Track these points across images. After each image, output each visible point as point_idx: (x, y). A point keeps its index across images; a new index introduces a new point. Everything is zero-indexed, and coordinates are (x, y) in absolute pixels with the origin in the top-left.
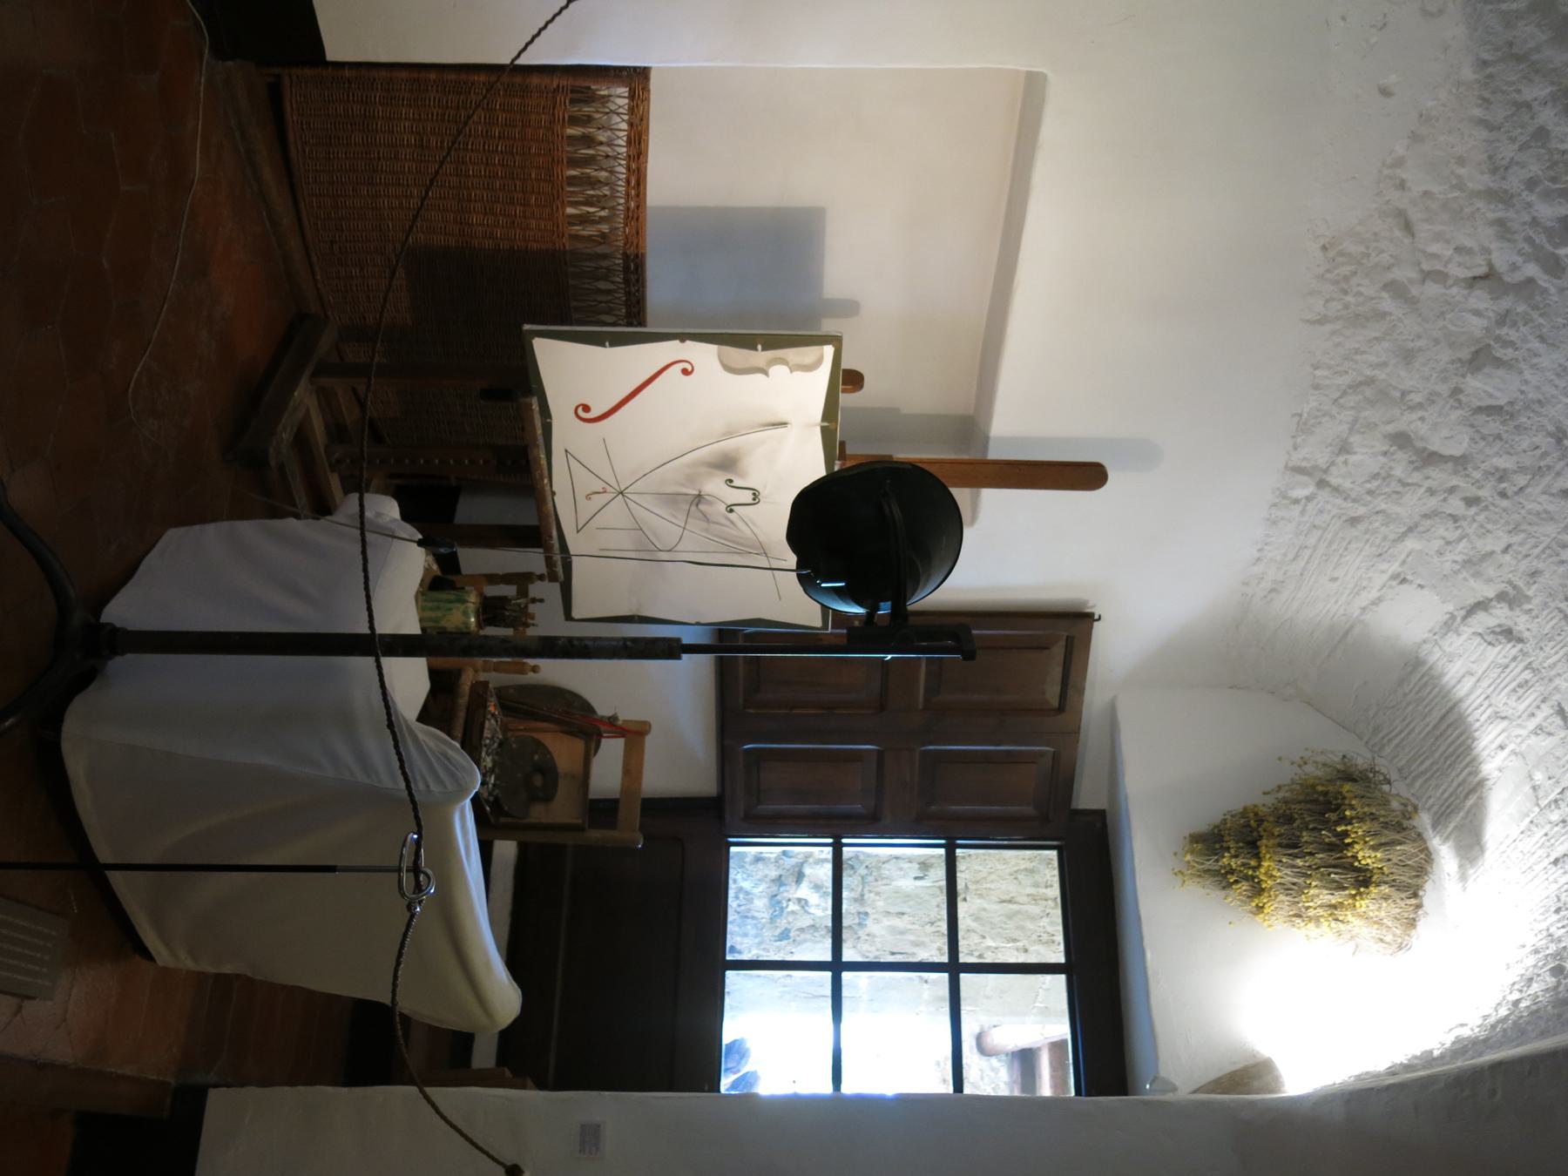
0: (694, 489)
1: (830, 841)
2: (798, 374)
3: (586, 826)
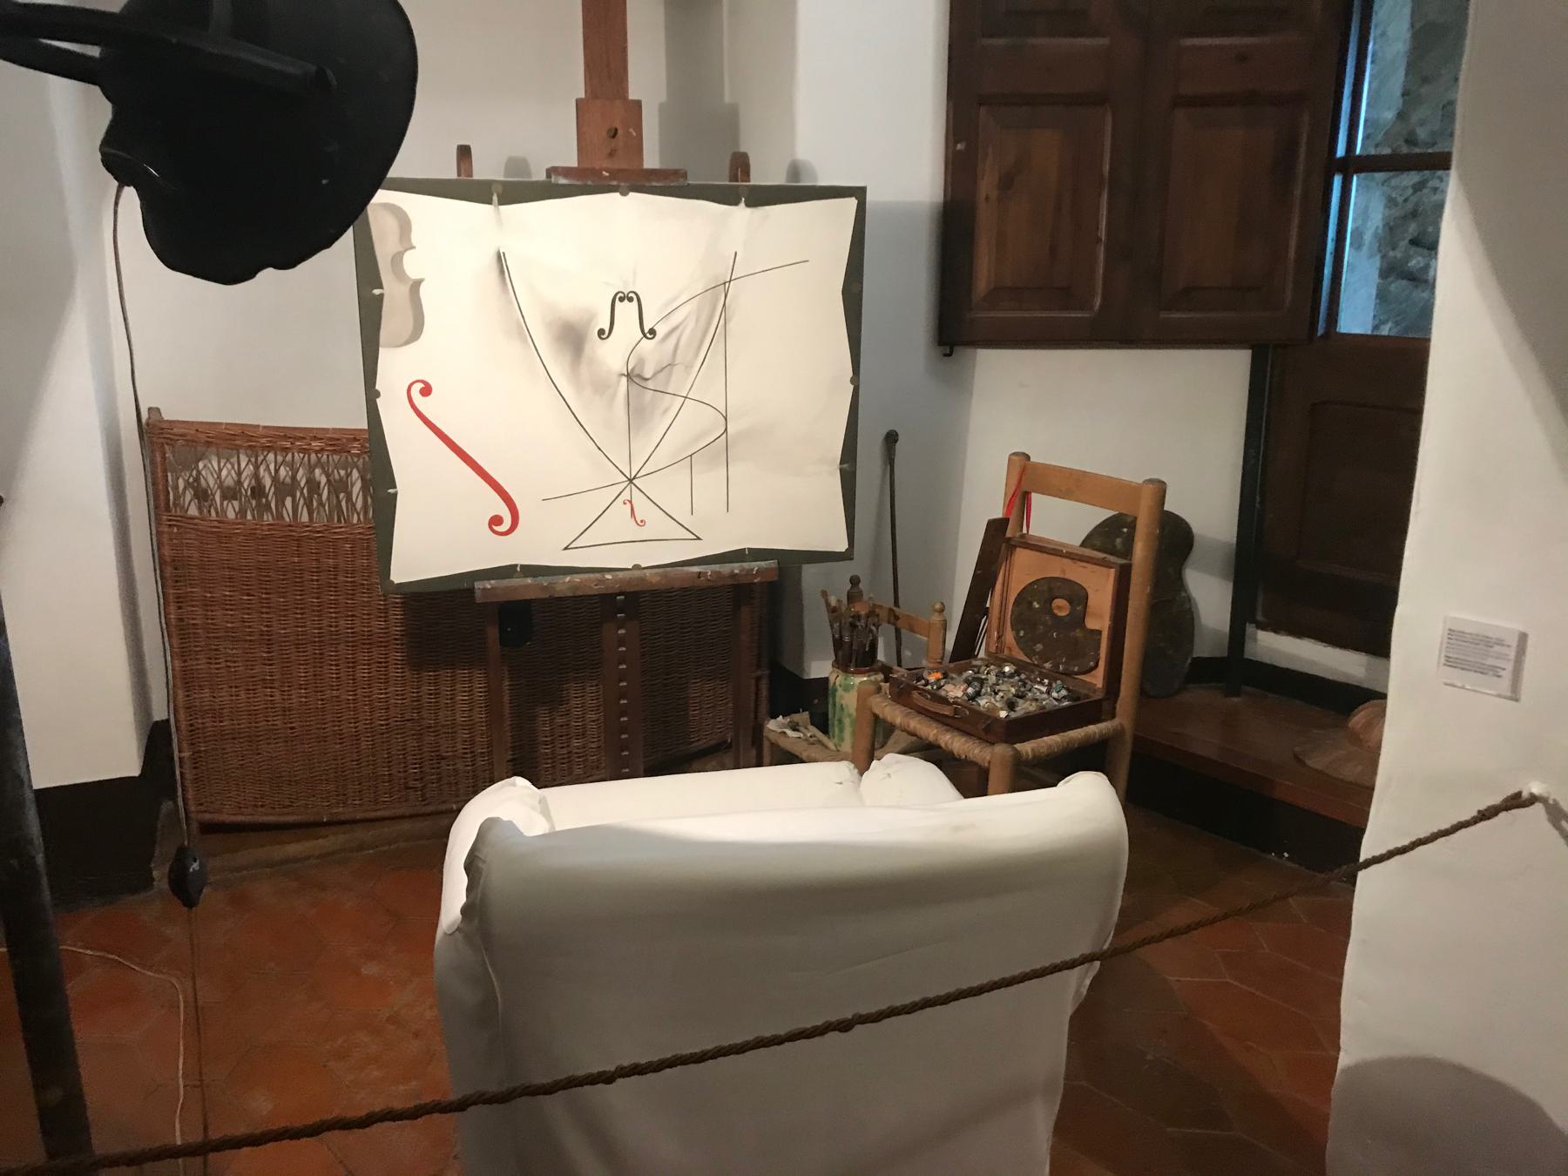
0: (619, 382)
1: (1337, 181)
2: (415, 238)
3: (1124, 561)
